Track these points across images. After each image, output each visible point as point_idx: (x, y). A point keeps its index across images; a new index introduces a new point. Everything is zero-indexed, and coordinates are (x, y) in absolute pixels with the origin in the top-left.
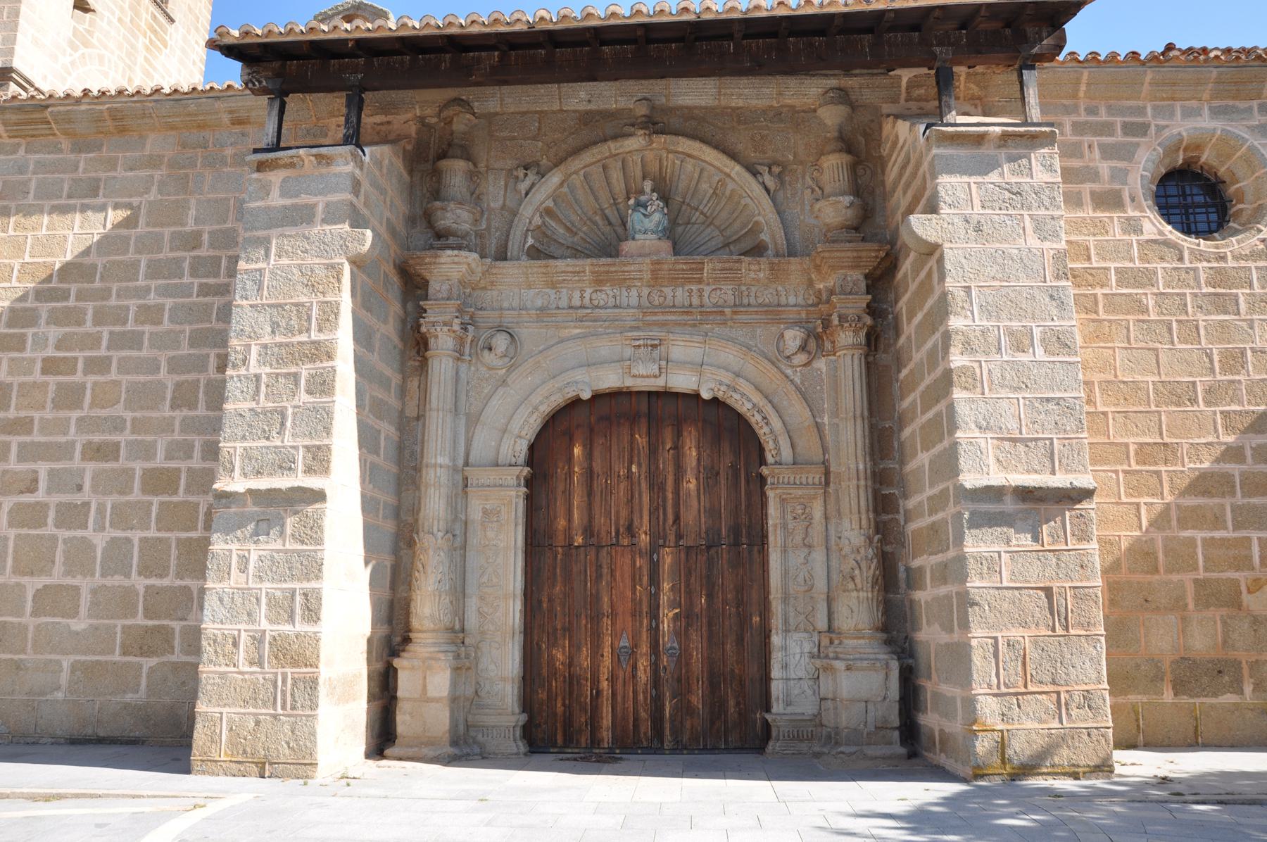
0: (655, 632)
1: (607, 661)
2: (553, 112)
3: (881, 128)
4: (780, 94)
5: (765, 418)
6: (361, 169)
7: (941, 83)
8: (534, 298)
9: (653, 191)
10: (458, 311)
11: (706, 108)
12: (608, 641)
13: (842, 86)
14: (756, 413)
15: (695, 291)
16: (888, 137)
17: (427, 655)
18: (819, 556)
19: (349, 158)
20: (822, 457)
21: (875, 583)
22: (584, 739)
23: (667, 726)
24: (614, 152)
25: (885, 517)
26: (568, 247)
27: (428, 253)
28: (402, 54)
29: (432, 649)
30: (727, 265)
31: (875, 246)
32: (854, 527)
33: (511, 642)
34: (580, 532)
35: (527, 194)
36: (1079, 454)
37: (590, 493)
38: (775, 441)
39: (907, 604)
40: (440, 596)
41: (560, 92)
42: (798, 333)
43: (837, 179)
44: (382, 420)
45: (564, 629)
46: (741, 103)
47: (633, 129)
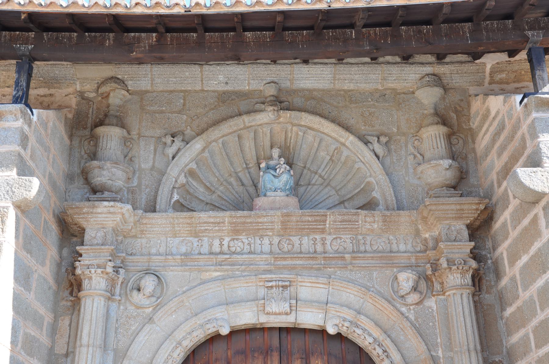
2: (196, 92)
3: (469, 105)
4: (384, 79)
5: (385, 351)
6: (30, 125)
7: (534, 60)
9: (280, 157)
10: (111, 255)
11: (323, 90)
13: (436, 72)
14: (377, 347)
15: (318, 240)
16: (477, 113)
19: (19, 115)
24: (247, 124)
26: (207, 203)
27: (87, 204)
28: (69, 30)
30: (346, 218)
31: (476, 200)
35: (173, 158)
41: (202, 75)
42: (411, 275)
43: (435, 147)
46: (352, 86)
47: (263, 106)
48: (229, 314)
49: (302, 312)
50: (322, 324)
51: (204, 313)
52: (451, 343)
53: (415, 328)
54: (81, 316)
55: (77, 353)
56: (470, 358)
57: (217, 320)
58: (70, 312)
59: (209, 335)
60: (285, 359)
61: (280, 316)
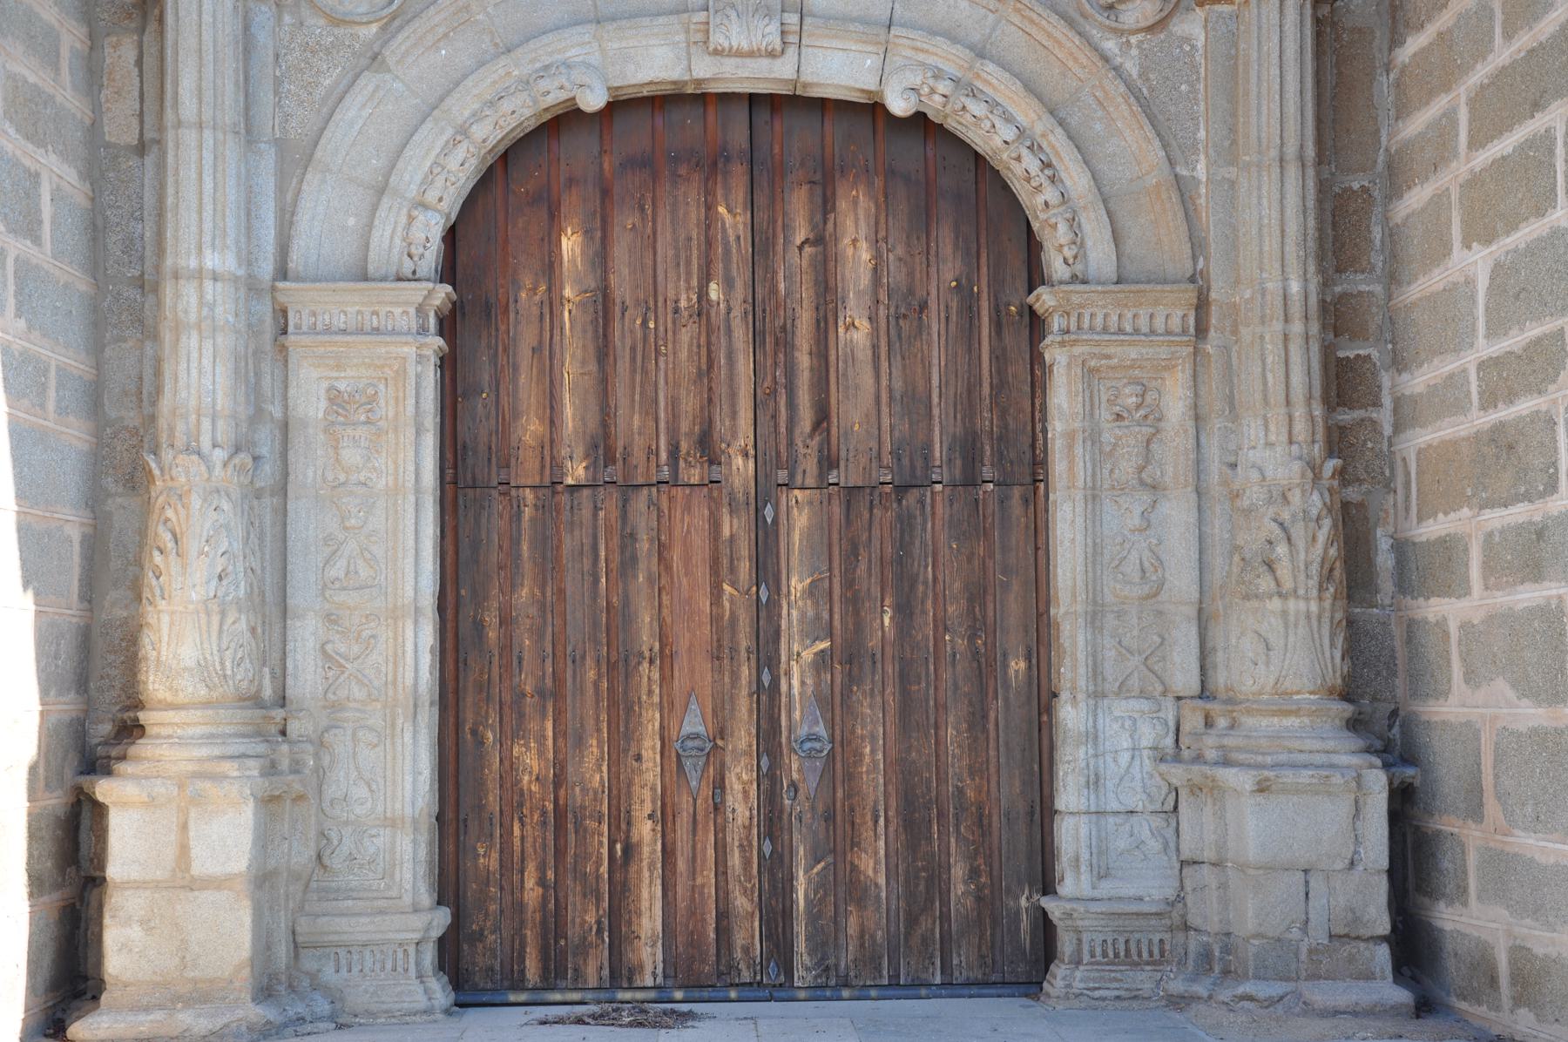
0: (768, 698)
1: (651, 770)
5: (1047, 165)
12: (651, 721)
14: (1025, 152)
17: (191, 767)
18: (1177, 512)
20: (1189, 264)
21: (1327, 576)
22: (595, 967)
23: (800, 929)
25: (1346, 416)
29: (204, 752)
32: (1273, 438)
33: (409, 728)
34: (579, 451)
37: (603, 352)
38: (1072, 222)
39: (1397, 632)
40: (223, 614)
44: (41, 144)
45: (541, 693)
48: (603, 51)
49: (816, 50)
50: (872, 85)
51: (532, 45)
52: (1234, 142)
53: (1137, 99)
54: (170, 35)
55: (171, 145)
56: (1282, 181)
57: (569, 67)
58: (133, 25)
59: (546, 110)
60: (765, 184)
61: (753, 60)
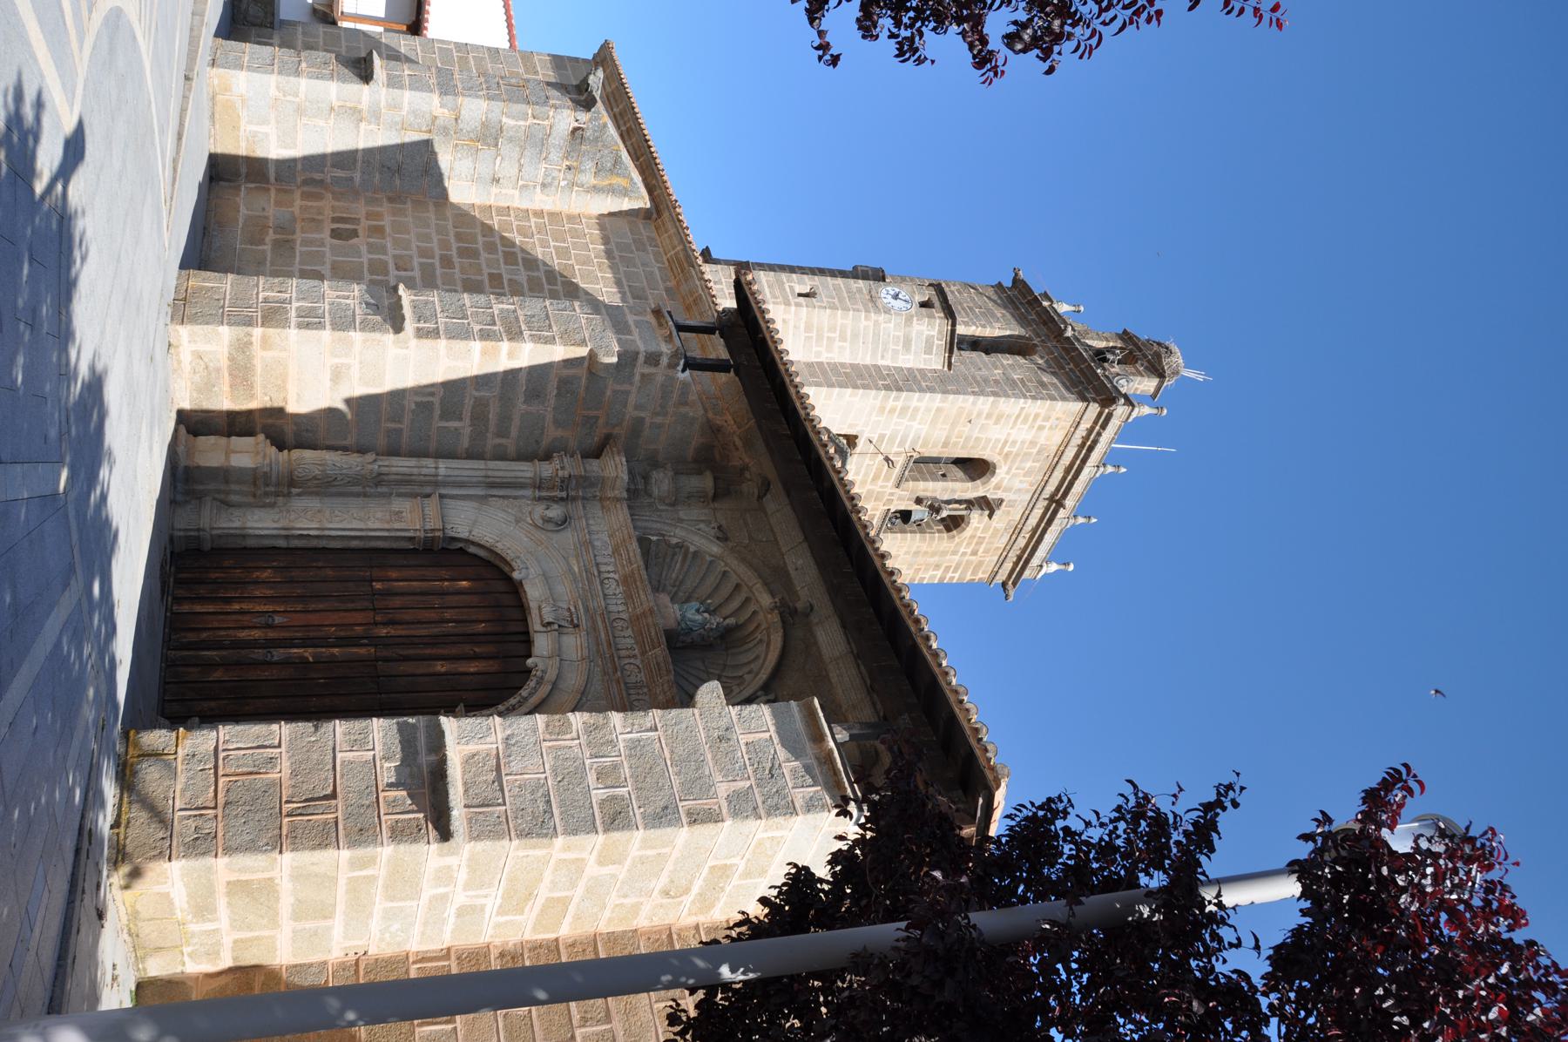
2: (779, 549)
8: (602, 540)
24: (754, 589)
26: (659, 581)
30: (662, 665)
36: (490, 831)
46: (834, 680)
